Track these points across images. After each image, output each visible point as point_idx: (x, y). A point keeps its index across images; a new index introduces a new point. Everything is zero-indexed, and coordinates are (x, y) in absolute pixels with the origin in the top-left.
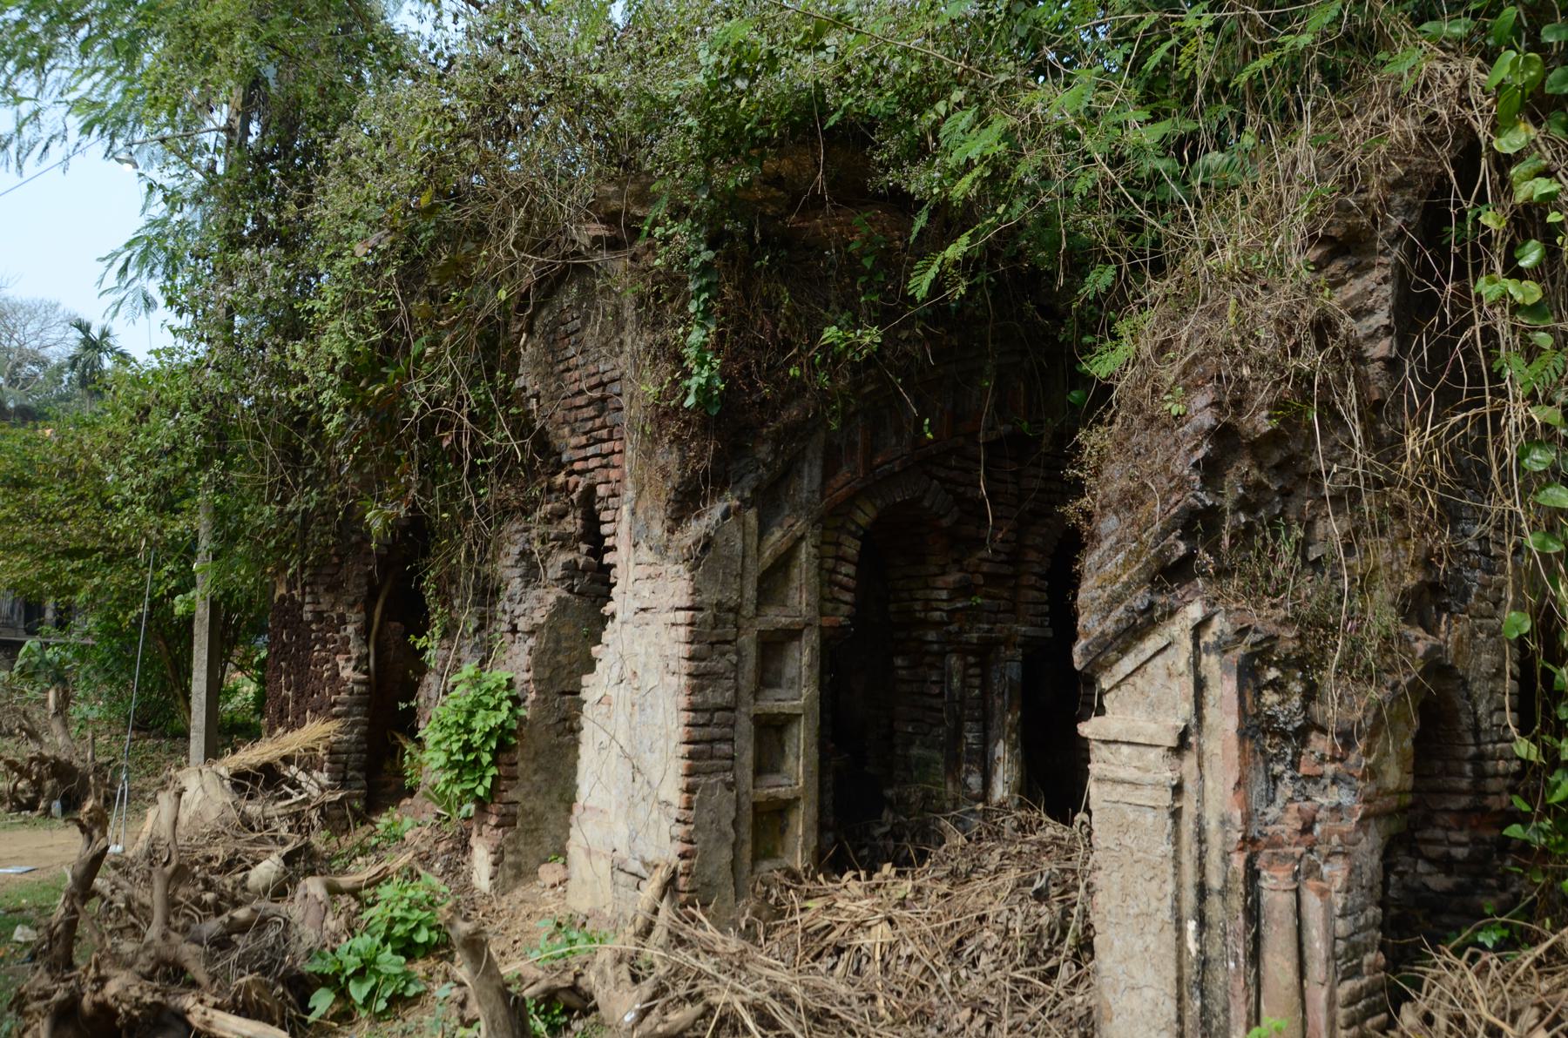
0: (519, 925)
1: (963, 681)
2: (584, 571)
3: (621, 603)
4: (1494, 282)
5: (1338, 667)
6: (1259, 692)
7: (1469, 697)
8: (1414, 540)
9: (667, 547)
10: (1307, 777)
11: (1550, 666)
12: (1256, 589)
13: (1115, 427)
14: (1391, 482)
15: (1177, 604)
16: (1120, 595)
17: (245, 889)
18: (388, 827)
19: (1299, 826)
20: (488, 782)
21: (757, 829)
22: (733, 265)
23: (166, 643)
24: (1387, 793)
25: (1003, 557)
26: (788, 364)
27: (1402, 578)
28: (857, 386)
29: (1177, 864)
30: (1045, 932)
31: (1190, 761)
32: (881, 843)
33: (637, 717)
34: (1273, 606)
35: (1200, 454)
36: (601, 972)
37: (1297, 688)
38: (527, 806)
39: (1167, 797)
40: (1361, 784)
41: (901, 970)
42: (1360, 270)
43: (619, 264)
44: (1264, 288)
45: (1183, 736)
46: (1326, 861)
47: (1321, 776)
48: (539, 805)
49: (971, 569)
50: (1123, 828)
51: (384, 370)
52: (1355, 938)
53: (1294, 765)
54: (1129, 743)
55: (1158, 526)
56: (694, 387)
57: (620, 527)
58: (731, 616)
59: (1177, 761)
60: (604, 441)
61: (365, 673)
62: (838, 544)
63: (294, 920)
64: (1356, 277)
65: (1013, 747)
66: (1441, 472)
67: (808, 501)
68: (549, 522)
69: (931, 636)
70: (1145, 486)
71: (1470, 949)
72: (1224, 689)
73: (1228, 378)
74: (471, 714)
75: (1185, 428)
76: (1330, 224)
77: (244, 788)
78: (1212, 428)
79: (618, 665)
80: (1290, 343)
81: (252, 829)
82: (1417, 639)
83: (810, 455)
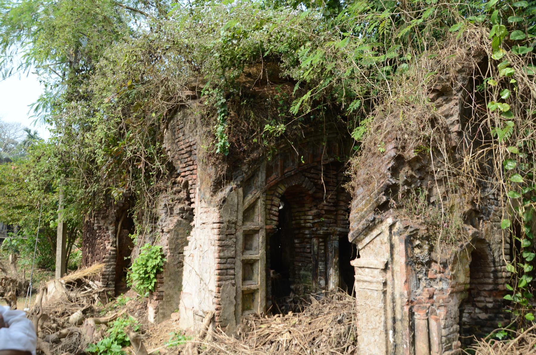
0: (163, 334)
1: (318, 247)
2: (187, 211)
3: (197, 221)
4: (494, 104)
5: (441, 239)
6: (413, 248)
7: (491, 250)
8: (467, 194)
9: (211, 202)
10: (431, 279)
11: (518, 238)
12: (411, 212)
13: (363, 157)
14: (459, 174)
15: (383, 218)
16: (364, 216)
17: (68, 323)
18: (120, 301)
19: (428, 296)
20: (153, 284)
21: (244, 300)
22: (234, 104)
23: (51, 238)
24: (460, 284)
25: (332, 204)
26: (253, 138)
27: (464, 208)
28: (277, 145)
29: (385, 310)
30: (342, 335)
31: (389, 274)
32: (289, 305)
33: (201, 261)
34: (418, 218)
35: (390, 165)
36: (187, 351)
37: (426, 247)
38: (167, 293)
39: (381, 286)
40: (450, 281)
41: (293, 349)
42: (447, 101)
43: (195, 104)
44: (413, 107)
45: (387, 265)
46: (438, 309)
47: (436, 278)
48: (171, 292)
49: (320, 208)
50: (367, 298)
51: (118, 142)
52: (449, 336)
53: (426, 275)
54: (368, 268)
55: (376, 191)
56: (219, 146)
57: (196, 196)
58: (233, 225)
59: (385, 274)
60: (191, 165)
61: (115, 247)
62: (272, 200)
63: (83, 333)
64: (446, 103)
65: (336, 270)
66: (475, 170)
67: (261, 185)
68: (175, 194)
69: (307, 232)
70: (372, 177)
71: (491, 340)
72: (400, 248)
73: (400, 139)
74: (147, 261)
75: (385, 156)
76: (436, 85)
77: (70, 287)
78: (394, 156)
79: (195, 242)
80: (421, 126)
81: (72, 302)
82: (469, 229)
83: (261, 169)
